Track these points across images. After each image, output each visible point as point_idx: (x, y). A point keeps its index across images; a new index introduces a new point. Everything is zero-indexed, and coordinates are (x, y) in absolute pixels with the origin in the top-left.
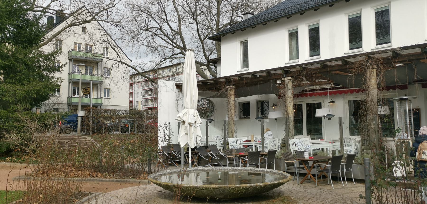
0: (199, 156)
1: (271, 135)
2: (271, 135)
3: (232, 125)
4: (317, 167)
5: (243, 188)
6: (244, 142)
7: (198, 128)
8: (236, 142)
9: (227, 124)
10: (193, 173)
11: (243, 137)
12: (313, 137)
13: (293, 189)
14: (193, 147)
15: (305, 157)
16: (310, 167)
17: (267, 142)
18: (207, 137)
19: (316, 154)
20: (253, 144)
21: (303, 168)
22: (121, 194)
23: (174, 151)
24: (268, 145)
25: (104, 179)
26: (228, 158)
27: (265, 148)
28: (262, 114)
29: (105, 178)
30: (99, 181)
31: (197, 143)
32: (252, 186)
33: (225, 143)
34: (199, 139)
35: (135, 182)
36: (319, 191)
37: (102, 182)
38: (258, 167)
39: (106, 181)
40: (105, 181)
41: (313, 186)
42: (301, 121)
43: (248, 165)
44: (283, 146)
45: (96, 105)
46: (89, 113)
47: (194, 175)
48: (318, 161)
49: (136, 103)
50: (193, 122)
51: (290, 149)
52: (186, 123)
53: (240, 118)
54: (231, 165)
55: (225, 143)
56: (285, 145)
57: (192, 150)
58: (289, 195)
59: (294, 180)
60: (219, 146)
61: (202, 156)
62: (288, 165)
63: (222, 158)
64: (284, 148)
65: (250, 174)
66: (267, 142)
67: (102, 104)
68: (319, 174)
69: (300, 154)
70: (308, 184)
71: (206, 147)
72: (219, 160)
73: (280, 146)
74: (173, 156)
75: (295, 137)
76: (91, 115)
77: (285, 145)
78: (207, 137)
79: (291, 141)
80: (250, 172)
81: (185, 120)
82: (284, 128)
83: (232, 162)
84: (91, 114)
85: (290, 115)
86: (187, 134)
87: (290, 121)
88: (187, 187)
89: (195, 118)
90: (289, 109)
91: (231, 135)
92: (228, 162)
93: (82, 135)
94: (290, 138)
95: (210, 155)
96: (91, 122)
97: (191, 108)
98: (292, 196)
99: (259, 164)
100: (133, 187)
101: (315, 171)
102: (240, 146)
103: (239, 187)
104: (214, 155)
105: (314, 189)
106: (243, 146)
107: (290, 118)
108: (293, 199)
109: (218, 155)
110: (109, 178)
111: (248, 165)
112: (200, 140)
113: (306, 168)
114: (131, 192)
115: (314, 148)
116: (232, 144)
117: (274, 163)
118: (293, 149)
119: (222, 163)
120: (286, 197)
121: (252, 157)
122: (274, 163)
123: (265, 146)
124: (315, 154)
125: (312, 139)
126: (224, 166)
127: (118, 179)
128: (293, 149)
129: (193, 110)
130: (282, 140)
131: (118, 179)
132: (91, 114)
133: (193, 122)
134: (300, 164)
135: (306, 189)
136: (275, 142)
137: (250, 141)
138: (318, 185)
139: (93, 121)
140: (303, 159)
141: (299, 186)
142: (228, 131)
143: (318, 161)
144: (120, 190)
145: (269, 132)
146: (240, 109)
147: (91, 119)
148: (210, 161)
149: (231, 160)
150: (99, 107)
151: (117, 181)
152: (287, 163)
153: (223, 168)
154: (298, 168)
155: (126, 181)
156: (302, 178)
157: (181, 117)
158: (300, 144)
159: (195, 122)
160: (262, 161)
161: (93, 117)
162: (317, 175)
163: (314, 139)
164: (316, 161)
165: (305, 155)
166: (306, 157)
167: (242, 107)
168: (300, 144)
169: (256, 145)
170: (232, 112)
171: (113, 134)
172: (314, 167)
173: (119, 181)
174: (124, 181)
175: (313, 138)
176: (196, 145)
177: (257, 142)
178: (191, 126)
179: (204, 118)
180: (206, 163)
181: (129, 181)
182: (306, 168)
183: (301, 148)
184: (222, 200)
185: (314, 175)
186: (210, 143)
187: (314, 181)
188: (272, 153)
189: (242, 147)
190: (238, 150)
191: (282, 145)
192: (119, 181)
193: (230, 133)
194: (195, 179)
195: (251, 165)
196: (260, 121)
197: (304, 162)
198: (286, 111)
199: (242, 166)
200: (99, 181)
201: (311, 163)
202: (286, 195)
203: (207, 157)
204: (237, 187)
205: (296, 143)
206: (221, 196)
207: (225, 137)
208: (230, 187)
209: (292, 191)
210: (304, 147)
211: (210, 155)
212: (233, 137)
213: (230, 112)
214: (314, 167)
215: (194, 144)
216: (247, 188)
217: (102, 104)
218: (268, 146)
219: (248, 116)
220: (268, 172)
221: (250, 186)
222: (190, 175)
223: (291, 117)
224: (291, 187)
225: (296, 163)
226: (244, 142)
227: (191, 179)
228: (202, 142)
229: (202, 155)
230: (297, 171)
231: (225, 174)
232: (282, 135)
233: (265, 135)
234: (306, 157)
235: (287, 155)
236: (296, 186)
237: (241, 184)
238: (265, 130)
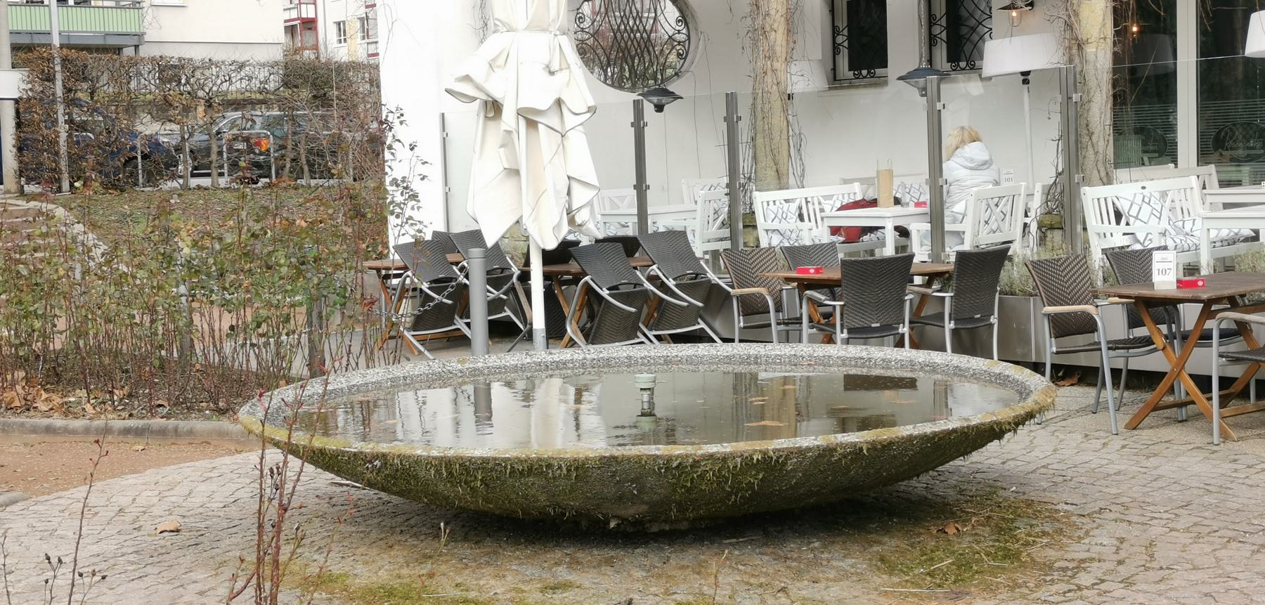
0: (589, 290)
1: (985, 165)
2: (985, 165)
3: (777, 120)
4: (1224, 334)
5: (749, 463)
6: (843, 208)
7: (578, 142)
8: (800, 213)
9: (744, 110)
10: (557, 382)
11: (846, 182)
12: (1231, 172)
13: (1079, 459)
14: (552, 245)
15: (1156, 278)
16: (1185, 337)
17: (959, 208)
18: (641, 187)
19: (1229, 269)
20: (886, 217)
21: (1147, 341)
22: (124, 501)
23: (653, 279)
24: (969, 221)
25: (58, 421)
26: (742, 299)
27: (948, 240)
28: (954, 57)
29: (66, 414)
30: (34, 430)
31: (572, 221)
32: (801, 452)
33: (740, 220)
34: (581, 196)
35: (222, 434)
36: (1227, 467)
37: (48, 438)
38: (900, 344)
39: (73, 432)
40: (66, 431)
41: (1198, 439)
42: (1164, 87)
43: (841, 335)
44: (1052, 228)
45: (112, 41)
46: (50, 79)
47: (564, 392)
48: (1233, 302)
49: (334, 29)
50: (544, 103)
51: (1087, 242)
52: (509, 114)
53: (835, 80)
54: (756, 333)
55: (740, 220)
56: (1061, 216)
57: (548, 257)
58: (1048, 496)
59: (1097, 408)
60: (704, 239)
61: (605, 293)
62: (1063, 327)
63: (715, 299)
64: (1057, 235)
65: (855, 383)
66: (959, 208)
67: (140, 36)
68: (1236, 371)
69: (1130, 263)
70: (1173, 433)
71: (629, 245)
72: (697, 314)
73: (1034, 228)
74: (454, 299)
75: (1122, 173)
76: (59, 91)
77: (1061, 216)
78: (641, 187)
79: (1092, 197)
80: (853, 371)
81: (498, 95)
82: (1054, 128)
83: (757, 320)
84: (59, 83)
85: (1090, 50)
86: (516, 172)
87: (1092, 83)
88: (428, 462)
89: (561, 77)
90: (1085, 12)
91: (771, 173)
92: (739, 322)
93: (21, 193)
94: (1086, 181)
95: (648, 286)
96: (63, 129)
97: (536, 26)
98: (1064, 499)
99: (904, 329)
100: (205, 464)
101: (1210, 360)
102: (815, 234)
103: (724, 459)
104: (671, 283)
105: (1201, 455)
106: (835, 231)
107: (1089, 70)
108: (1068, 515)
109: (696, 284)
110: (89, 411)
111: (841, 335)
112: (590, 204)
113: (1159, 342)
114: (181, 490)
115: (1224, 233)
116: (776, 225)
117: (994, 320)
118: (1103, 237)
119: (717, 325)
120: (1030, 504)
121: (865, 286)
122: (994, 320)
123: (948, 227)
124: (1226, 266)
125: (1224, 184)
126: (725, 340)
127: (132, 423)
128: (1103, 237)
129: (544, 39)
130: (1048, 191)
131: (132, 423)
132: (59, 83)
133: (544, 103)
134: (1134, 322)
135: (1153, 461)
136: (1005, 206)
137: (873, 203)
138: (1225, 436)
139: (70, 121)
140: (1145, 292)
141: (1117, 443)
142: (755, 150)
143: (1233, 302)
144: (131, 480)
145: (975, 151)
146: (835, 31)
147: (61, 109)
148: (648, 314)
149: (752, 307)
150: (128, 52)
151: (127, 431)
152: (1055, 320)
153: (721, 349)
154: (1114, 345)
155: (176, 430)
156: (1137, 399)
157: (479, 79)
158: (1146, 209)
159: (559, 102)
160: (928, 311)
161: (71, 102)
162: (1225, 382)
163: (1238, 183)
164: (1218, 300)
165: (1156, 266)
166: (1164, 279)
167: (842, 23)
168: (1146, 209)
169: (900, 223)
170: (772, 48)
171: (186, 187)
172: (1207, 336)
173: (139, 432)
174: (162, 432)
175: (1234, 177)
176: (564, 232)
177: (912, 209)
178: (532, 124)
179: (618, 84)
180: (627, 330)
181: (191, 432)
182: (1159, 342)
183: (1145, 229)
184: (655, 529)
185: (1203, 382)
186: (660, 222)
187: (1202, 416)
188: (982, 266)
189: (825, 238)
190: (796, 254)
191: (1047, 222)
192: (139, 432)
193: (766, 161)
194: (552, 409)
195: (859, 334)
196: (923, 91)
197: (1151, 309)
198: (1069, 26)
199: (812, 340)
200: (34, 430)
201: (1189, 314)
202: (1033, 496)
203: (636, 296)
204: (711, 456)
205: (1123, 206)
206: (632, 511)
207: (736, 189)
208: (669, 459)
209: (1070, 473)
210: (1164, 224)
211: (648, 286)
212: (782, 187)
213: (763, 45)
214: (1207, 336)
215: (557, 228)
216: (770, 465)
217: (140, 36)
218: (967, 227)
219: (879, 71)
220: (959, 372)
221: (790, 453)
222: (539, 394)
223: (1100, 57)
224: (1063, 444)
225: (1111, 320)
226: (843, 208)
227: (546, 419)
228: (603, 214)
229: (602, 290)
230: (1108, 361)
231: (744, 383)
232: (1045, 164)
233: (953, 168)
234: (1164, 279)
235: (1055, 278)
236: (1098, 444)
237: (844, 429)
238: (948, 140)
